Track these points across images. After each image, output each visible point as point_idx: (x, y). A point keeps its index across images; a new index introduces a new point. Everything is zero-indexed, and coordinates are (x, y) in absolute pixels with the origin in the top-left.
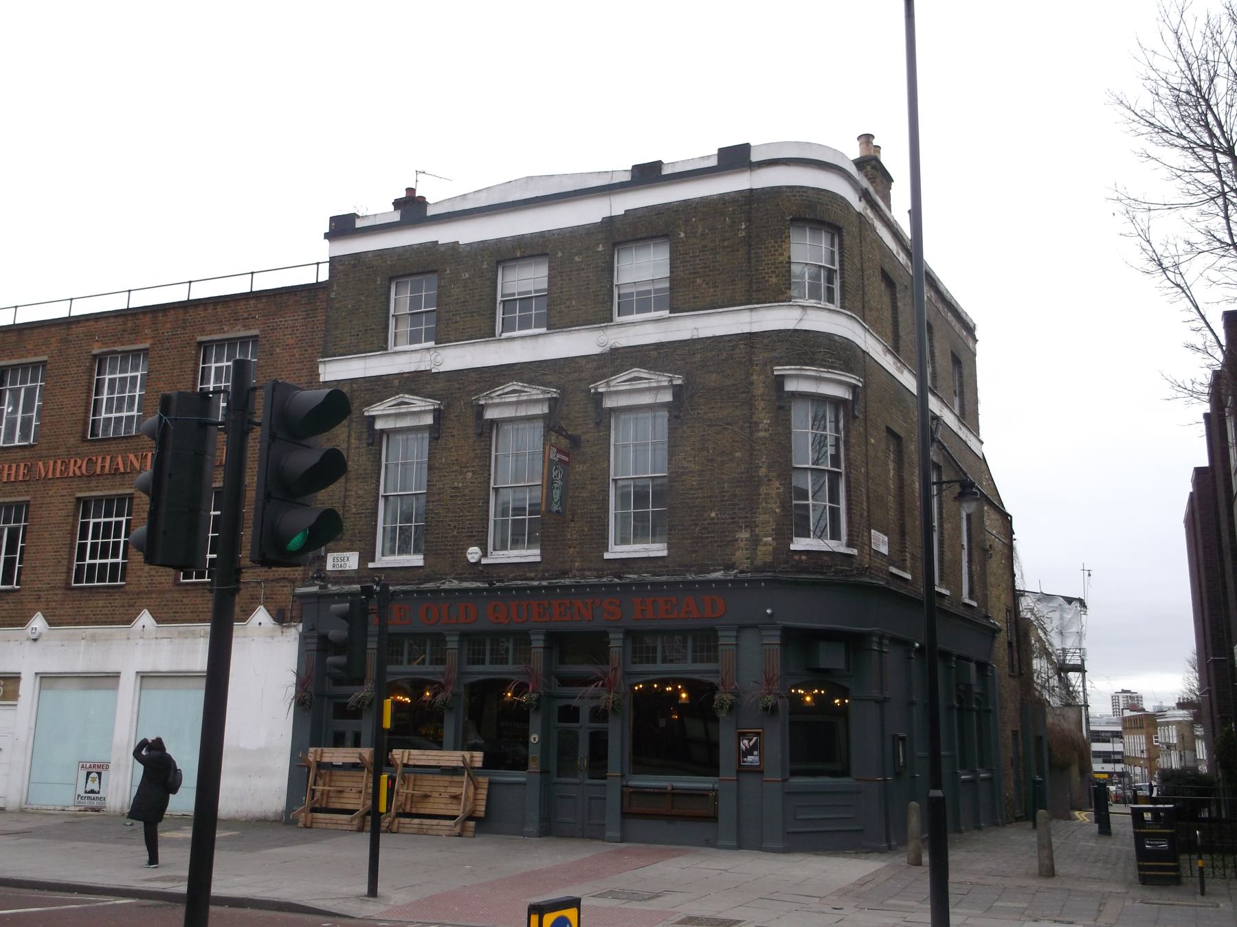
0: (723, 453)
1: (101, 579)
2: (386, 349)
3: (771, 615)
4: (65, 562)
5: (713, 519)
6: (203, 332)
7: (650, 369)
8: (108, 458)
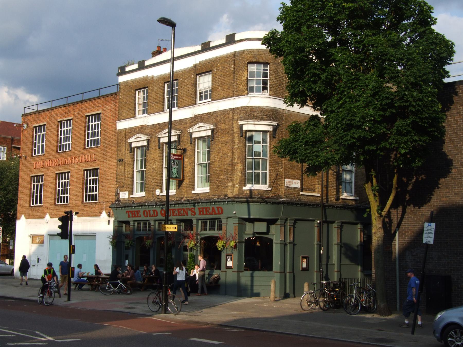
0: (225, 154)
1: (64, 202)
2: (135, 117)
3: (235, 214)
4: (54, 196)
5: (222, 178)
6: (87, 112)
7: (205, 123)
8: (83, 156)
